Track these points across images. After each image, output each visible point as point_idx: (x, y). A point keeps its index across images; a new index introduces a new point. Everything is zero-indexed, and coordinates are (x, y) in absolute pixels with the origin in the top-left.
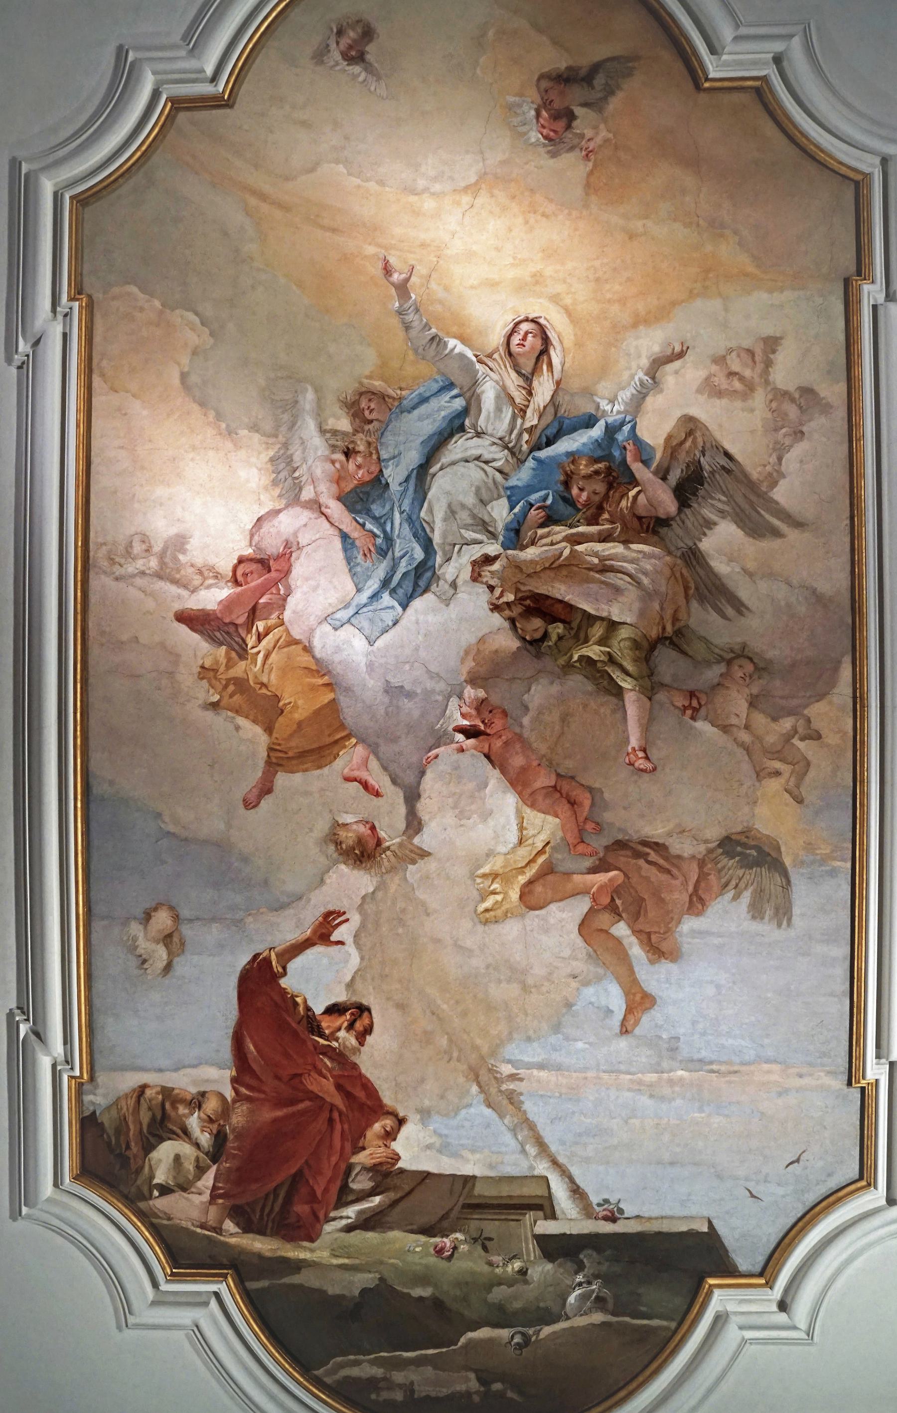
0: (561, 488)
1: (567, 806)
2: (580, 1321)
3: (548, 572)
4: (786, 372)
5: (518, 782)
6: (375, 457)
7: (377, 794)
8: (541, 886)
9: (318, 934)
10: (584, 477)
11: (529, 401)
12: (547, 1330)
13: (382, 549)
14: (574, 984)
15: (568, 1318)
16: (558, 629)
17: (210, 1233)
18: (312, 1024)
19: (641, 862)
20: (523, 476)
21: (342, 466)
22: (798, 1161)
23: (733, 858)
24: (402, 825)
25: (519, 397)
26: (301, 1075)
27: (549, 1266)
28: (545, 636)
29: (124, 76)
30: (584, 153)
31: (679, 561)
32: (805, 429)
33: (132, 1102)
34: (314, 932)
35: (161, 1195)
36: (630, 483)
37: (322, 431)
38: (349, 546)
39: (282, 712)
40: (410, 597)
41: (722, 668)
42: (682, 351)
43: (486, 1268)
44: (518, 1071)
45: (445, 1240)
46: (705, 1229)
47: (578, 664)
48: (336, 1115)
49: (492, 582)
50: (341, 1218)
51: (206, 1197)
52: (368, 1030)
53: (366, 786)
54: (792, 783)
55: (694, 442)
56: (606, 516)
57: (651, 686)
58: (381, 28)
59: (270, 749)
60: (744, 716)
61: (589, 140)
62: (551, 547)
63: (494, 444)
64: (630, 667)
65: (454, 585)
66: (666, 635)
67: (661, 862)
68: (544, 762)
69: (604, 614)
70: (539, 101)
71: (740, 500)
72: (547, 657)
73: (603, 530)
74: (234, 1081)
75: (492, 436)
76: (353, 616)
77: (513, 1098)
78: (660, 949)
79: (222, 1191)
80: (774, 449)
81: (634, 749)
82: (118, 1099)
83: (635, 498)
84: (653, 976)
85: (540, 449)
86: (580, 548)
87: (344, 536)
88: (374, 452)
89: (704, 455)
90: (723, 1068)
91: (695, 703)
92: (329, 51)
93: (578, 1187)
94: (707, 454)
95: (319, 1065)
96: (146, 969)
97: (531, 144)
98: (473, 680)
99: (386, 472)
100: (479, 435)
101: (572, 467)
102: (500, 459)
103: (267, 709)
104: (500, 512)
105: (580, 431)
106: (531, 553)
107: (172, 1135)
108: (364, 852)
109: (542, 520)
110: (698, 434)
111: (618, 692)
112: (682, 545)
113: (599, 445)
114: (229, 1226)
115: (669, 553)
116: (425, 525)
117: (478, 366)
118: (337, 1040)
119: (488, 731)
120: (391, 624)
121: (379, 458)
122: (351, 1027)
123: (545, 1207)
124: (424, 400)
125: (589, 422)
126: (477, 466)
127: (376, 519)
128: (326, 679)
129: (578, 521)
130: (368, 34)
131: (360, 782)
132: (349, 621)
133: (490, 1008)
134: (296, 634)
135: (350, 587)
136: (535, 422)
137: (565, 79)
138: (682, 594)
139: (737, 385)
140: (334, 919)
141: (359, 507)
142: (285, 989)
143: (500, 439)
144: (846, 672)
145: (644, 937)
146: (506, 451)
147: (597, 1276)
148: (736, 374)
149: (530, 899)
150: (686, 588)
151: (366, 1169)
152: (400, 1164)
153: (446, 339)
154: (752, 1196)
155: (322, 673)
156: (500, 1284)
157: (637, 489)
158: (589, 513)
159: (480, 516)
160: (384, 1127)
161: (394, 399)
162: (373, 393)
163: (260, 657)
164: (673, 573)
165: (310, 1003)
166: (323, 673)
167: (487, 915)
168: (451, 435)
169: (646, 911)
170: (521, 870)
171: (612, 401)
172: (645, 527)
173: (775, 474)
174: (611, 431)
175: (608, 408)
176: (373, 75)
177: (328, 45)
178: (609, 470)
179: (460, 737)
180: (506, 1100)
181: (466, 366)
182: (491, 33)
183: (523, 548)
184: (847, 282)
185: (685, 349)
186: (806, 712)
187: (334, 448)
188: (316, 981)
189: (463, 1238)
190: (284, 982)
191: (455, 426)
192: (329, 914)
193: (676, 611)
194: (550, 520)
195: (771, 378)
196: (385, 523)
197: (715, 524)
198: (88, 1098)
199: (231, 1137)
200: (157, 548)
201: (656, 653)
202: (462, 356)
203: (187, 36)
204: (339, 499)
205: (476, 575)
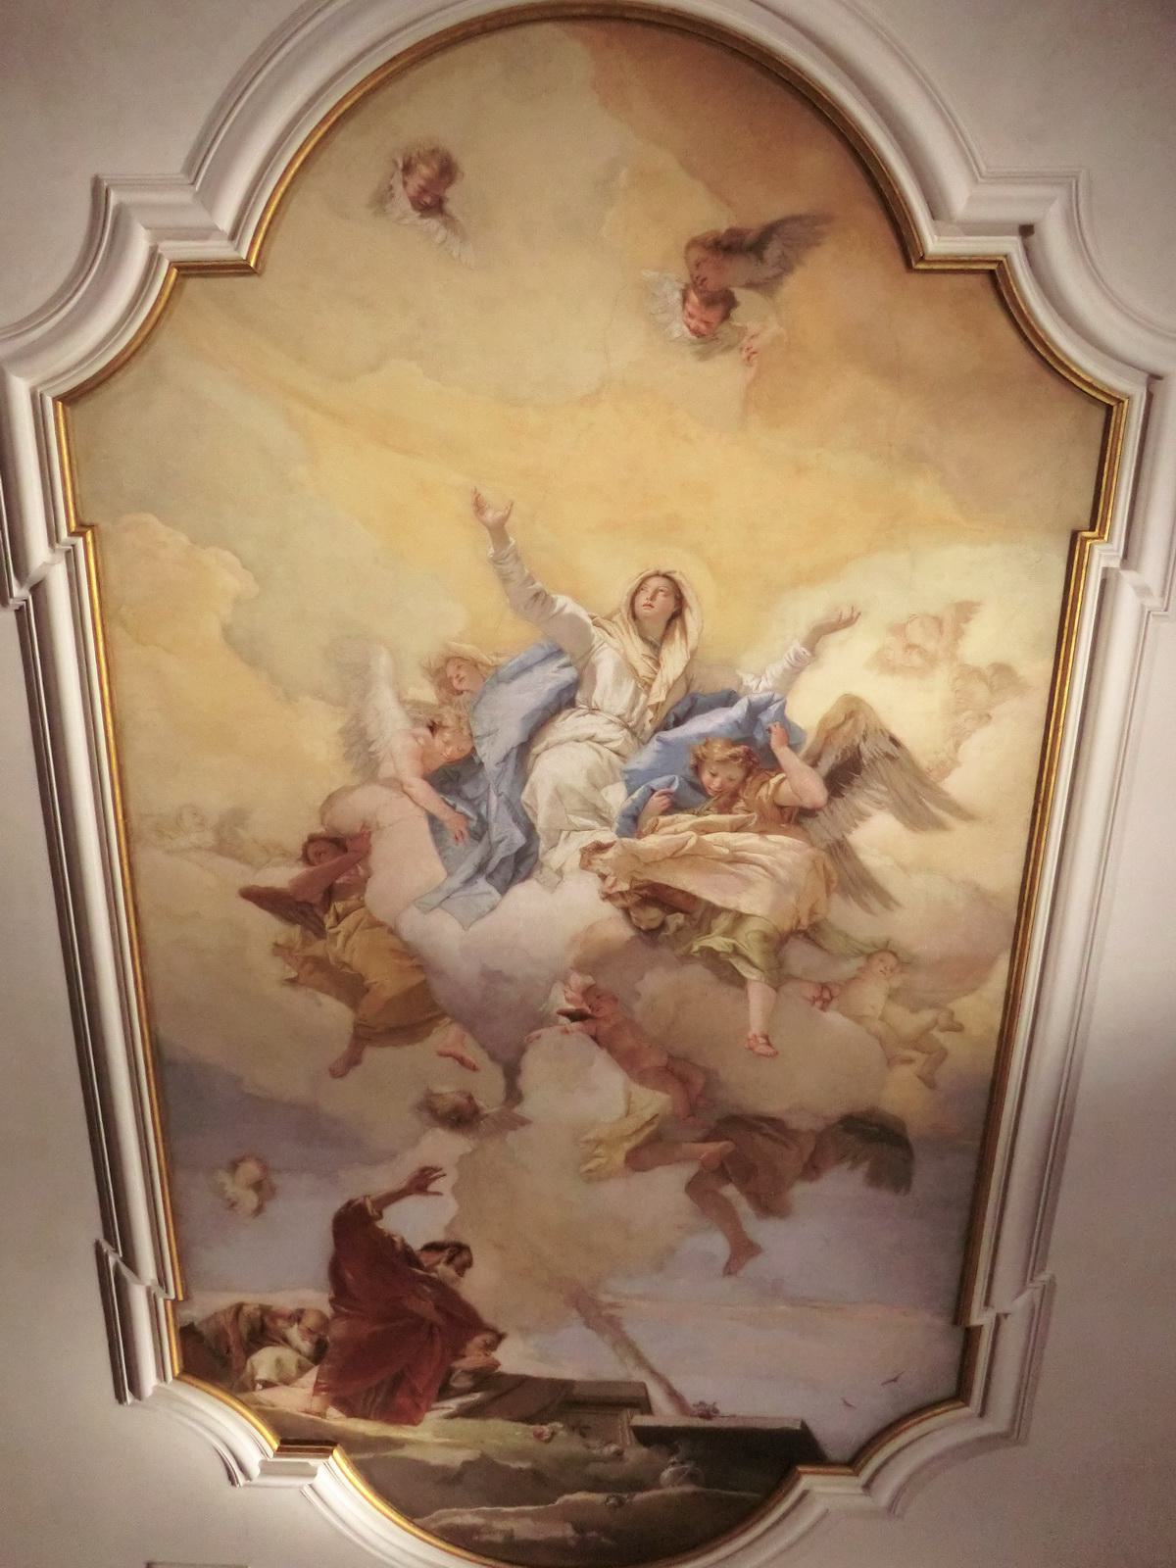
0: (689, 773)
3: (670, 861)
4: (981, 643)
6: (466, 732)
7: (474, 1069)
8: (650, 1149)
12: (639, 1497)
13: (476, 834)
15: (660, 1487)
16: (677, 920)
18: (409, 1257)
20: (645, 759)
22: (895, 1380)
25: (643, 668)
26: (401, 1298)
27: (644, 1450)
28: (663, 925)
29: (104, 228)
30: (744, 355)
31: (823, 854)
32: (992, 713)
33: (230, 1317)
34: (411, 1183)
36: (772, 770)
37: (402, 702)
39: (368, 990)
41: (860, 962)
42: (852, 618)
43: (584, 1449)
45: (544, 1427)
47: (698, 955)
49: (604, 871)
50: (443, 1408)
52: (469, 1264)
53: (462, 1061)
55: (855, 726)
56: (741, 804)
57: (779, 976)
58: (466, 163)
61: (752, 337)
62: (675, 836)
63: (611, 722)
64: (756, 959)
65: (560, 872)
66: (800, 928)
67: (776, 1134)
69: (732, 906)
70: (687, 279)
73: (736, 819)
74: (331, 1301)
75: (608, 712)
76: (444, 900)
78: (770, 1205)
85: (666, 728)
86: (708, 838)
87: (432, 819)
88: (465, 727)
92: (392, 196)
98: (581, 967)
99: (480, 751)
101: (704, 750)
102: (618, 740)
103: (351, 987)
104: (616, 798)
105: (717, 710)
106: (651, 842)
107: (273, 1342)
108: (461, 1118)
109: (666, 807)
110: (861, 717)
111: (741, 982)
112: (828, 837)
115: (812, 845)
116: (527, 809)
117: (594, 630)
119: (595, 1014)
120: (487, 909)
121: (471, 735)
122: (450, 1261)
123: (644, 1405)
124: (525, 669)
125: (728, 699)
126: (590, 746)
127: (469, 801)
128: (415, 962)
130: (447, 171)
132: (439, 905)
134: (380, 914)
136: (662, 698)
137: (727, 247)
138: (823, 889)
140: (431, 1174)
141: (447, 787)
143: (619, 717)
144: (1003, 967)
146: (625, 731)
147: (689, 1459)
149: (637, 1161)
151: (466, 1372)
152: (500, 1369)
153: (554, 596)
155: (410, 955)
157: (780, 776)
158: (721, 801)
159: (592, 801)
160: (485, 1341)
161: (489, 667)
163: (340, 939)
170: (628, 1138)
172: (786, 817)
173: (949, 762)
174: (755, 711)
175: (753, 684)
177: (391, 188)
178: (748, 755)
179: (564, 1020)
182: (624, 173)
183: (640, 836)
184: (1074, 535)
185: (855, 615)
186: (950, 1006)
187: (416, 721)
188: (414, 1224)
189: (561, 1426)
190: (381, 1225)
191: (565, 700)
193: (813, 905)
194: (675, 806)
196: (479, 805)
197: (870, 815)
199: (331, 1345)
202: (574, 618)
203: (192, 166)
205: (586, 863)
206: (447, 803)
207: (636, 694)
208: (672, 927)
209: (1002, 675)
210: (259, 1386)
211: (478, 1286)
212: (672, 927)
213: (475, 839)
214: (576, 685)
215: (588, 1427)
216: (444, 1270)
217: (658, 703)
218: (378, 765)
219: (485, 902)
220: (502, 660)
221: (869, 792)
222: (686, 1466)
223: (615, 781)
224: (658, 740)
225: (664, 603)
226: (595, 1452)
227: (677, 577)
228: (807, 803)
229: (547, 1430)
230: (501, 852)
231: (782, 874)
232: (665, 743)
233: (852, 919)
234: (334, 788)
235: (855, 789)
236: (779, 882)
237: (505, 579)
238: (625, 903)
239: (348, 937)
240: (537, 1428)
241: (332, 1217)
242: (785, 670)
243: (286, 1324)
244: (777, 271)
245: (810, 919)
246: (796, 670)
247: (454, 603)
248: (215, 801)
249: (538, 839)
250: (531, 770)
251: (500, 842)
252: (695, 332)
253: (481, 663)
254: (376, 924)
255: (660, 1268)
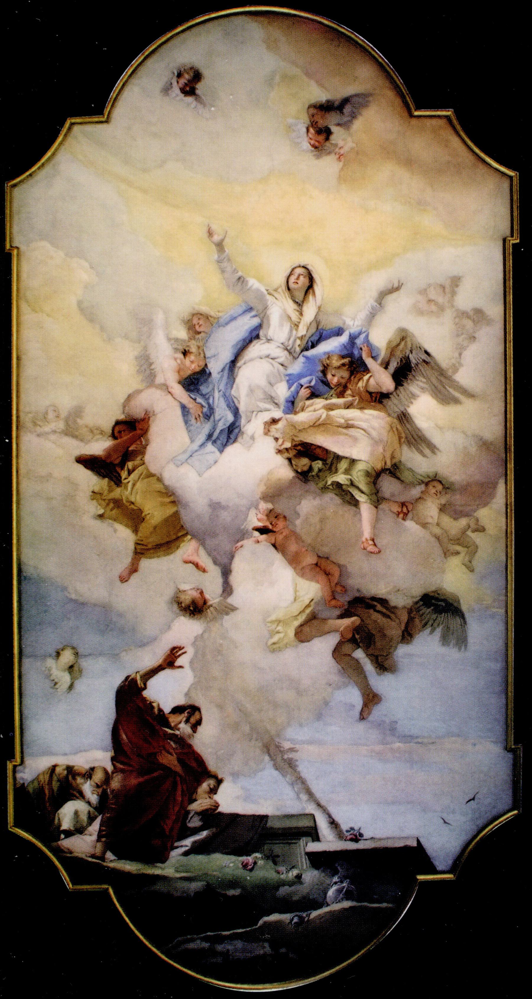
0: (321, 375)
1: (324, 576)
2: (337, 907)
3: (312, 428)
5: (294, 561)
6: (202, 355)
7: (204, 571)
8: (309, 626)
9: (168, 661)
10: (335, 368)
11: (300, 319)
12: (314, 914)
13: (207, 416)
14: (330, 689)
15: (328, 905)
16: (317, 465)
17: (97, 861)
18: (162, 718)
19: (371, 611)
20: (297, 367)
21: (182, 363)
22: (473, 799)
23: (429, 607)
24: (219, 590)
25: (294, 316)
27: (316, 872)
30: (337, 156)
31: (395, 420)
33: (47, 777)
34: (165, 660)
35: (66, 837)
36: (364, 371)
37: (169, 339)
38: (186, 413)
39: (144, 519)
40: (225, 445)
41: (423, 487)
44: (294, 746)
45: (249, 858)
46: (415, 844)
47: (331, 487)
48: (178, 779)
49: (277, 436)
50: (182, 846)
51: (95, 837)
52: (199, 722)
53: (197, 566)
54: (467, 559)
55: (406, 345)
56: (349, 392)
57: (377, 499)
58: (205, 72)
59: (137, 544)
60: (436, 518)
61: (340, 148)
64: (363, 487)
65: (253, 438)
66: (387, 467)
68: (310, 548)
69: (347, 455)
70: (308, 122)
71: (434, 380)
72: (311, 482)
74: (113, 759)
77: (291, 764)
78: (383, 665)
79: (104, 833)
80: (457, 349)
81: (367, 540)
82: (38, 776)
83: (368, 380)
84: (381, 683)
86: (332, 413)
87: (184, 408)
88: (202, 353)
89: (412, 353)
90: (425, 740)
91: (405, 510)
92: (172, 87)
93: (333, 820)
94: (414, 352)
95: (167, 746)
96: (57, 689)
97: (303, 151)
98: (266, 497)
99: (209, 366)
100: (269, 340)
102: (282, 357)
104: (282, 391)
106: (302, 417)
108: (195, 608)
111: (355, 503)
112: (397, 410)
113: (345, 347)
114: (109, 855)
115: (389, 415)
117: (268, 297)
118: (178, 729)
119: (275, 529)
120: (213, 463)
122: (187, 721)
123: (313, 834)
124: (233, 319)
125: (339, 332)
126: (268, 361)
127: (203, 396)
128: (172, 499)
129: (331, 396)
130: (197, 76)
131: (193, 563)
133: (276, 705)
135: (187, 440)
136: (304, 332)
137: (326, 108)
139: (433, 308)
140: (177, 652)
142: (145, 698)
143: (282, 344)
145: (373, 658)
146: (286, 352)
148: (433, 301)
149: (303, 634)
150: (400, 438)
151: (197, 813)
154: (445, 822)
155: (170, 496)
156: (284, 885)
157: (369, 375)
158: (338, 390)
159: (269, 393)
160: (209, 785)
161: (215, 318)
162: (201, 314)
163: (130, 485)
164: (392, 427)
165: (162, 706)
166: (169, 494)
167: (275, 646)
168: (251, 341)
169: (375, 642)
171: (354, 319)
172: (374, 399)
174: (353, 339)
176: (201, 103)
178: (351, 363)
179: (257, 534)
180: (286, 764)
181: (261, 298)
183: (296, 413)
185: (400, 284)
187: (176, 350)
188: (165, 692)
190: (145, 693)
191: (254, 336)
192: (174, 648)
193: (393, 452)
194: (314, 395)
195: (455, 304)
197: (418, 396)
198: (19, 775)
200: (64, 414)
201: (380, 479)
202: (258, 290)
204: (179, 382)
205: (266, 431)
206: (191, 398)
207: (291, 331)
208: (316, 470)
209: (478, 316)
210: (62, 836)
211: (206, 740)
212: (316, 470)
213: (206, 419)
214: (260, 326)
215: (278, 856)
216: (185, 729)
217: (302, 336)
218: (155, 376)
219: (211, 458)
220: (220, 314)
221: (417, 382)
222: (344, 885)
223: (281, 381)
224: (303, 356)
225: (303, 281)
226: (282, 876)
227: (309, 267)
228: (384, 390)
229: (251, 861)
230: (221, 426)
231: (374, 434)
232: (307, 358)
233: (417, 462)
234: (130, 391)
235: (409, 381)
236: (372, 439)
237: (223, 271)
238: (289, 455)
239: (134, 485)
240: (244, 858)
241: (116, 690)
242: (367, 315)
243: (82, 781)
244: (349, 118)
245: (391, 462)
246: (372, 316)
247: (197, 288)
248: (65, 402)
249: (241, 417)
250: (237, 375)
251: (220, 420)
252: (313, 146)
253: (211, 316)
254: (150, 475)
255: (319, 717)
